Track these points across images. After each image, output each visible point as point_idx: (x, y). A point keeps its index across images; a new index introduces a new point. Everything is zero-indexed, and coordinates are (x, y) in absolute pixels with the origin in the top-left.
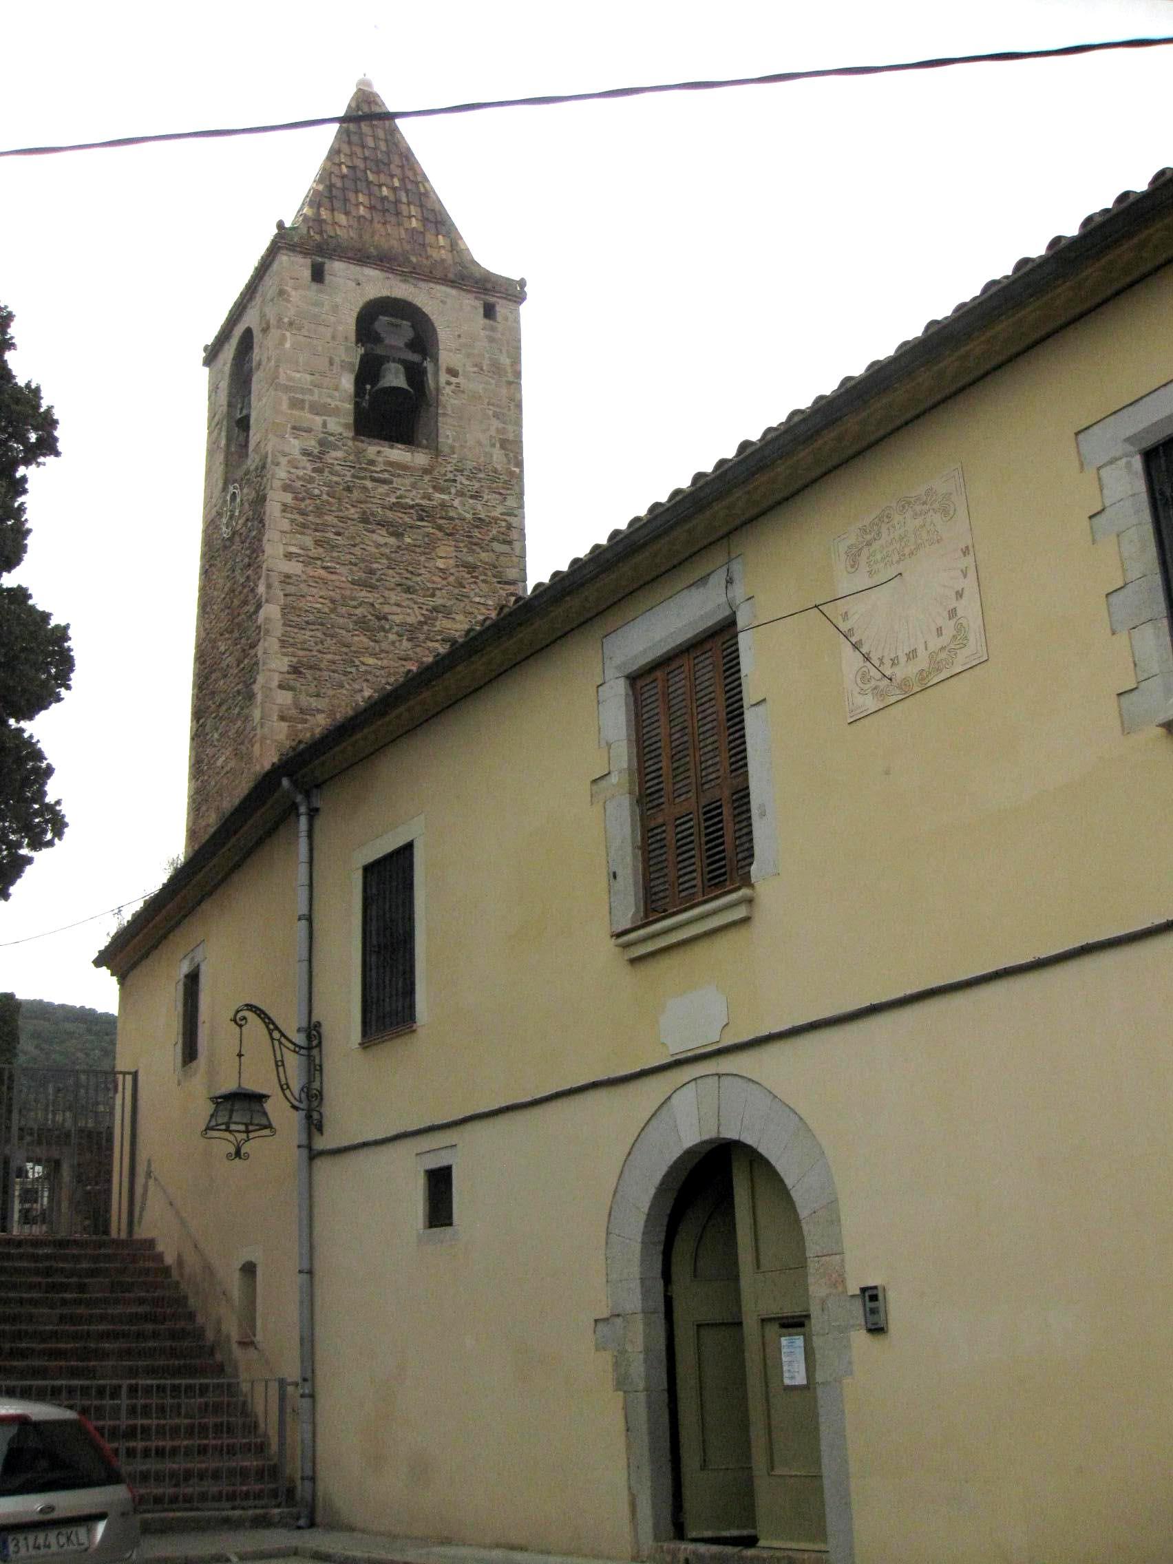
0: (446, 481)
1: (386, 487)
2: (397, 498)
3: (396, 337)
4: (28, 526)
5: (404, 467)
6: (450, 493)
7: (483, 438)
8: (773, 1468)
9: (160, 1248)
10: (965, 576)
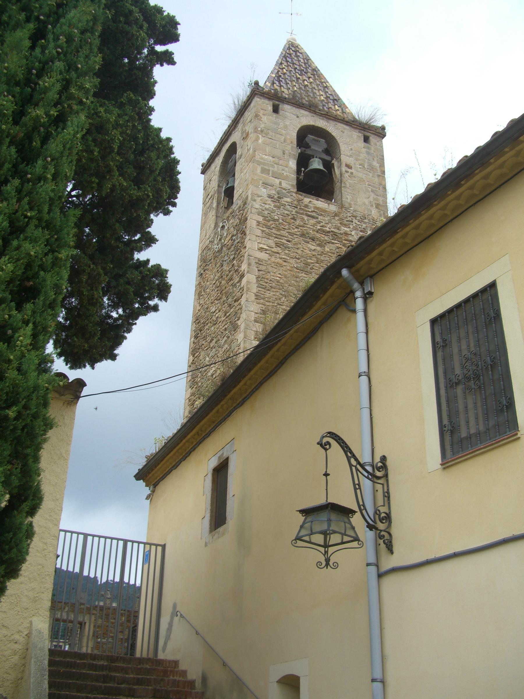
0: (347, 221)
5: (325, 211)
7: (367, 202)
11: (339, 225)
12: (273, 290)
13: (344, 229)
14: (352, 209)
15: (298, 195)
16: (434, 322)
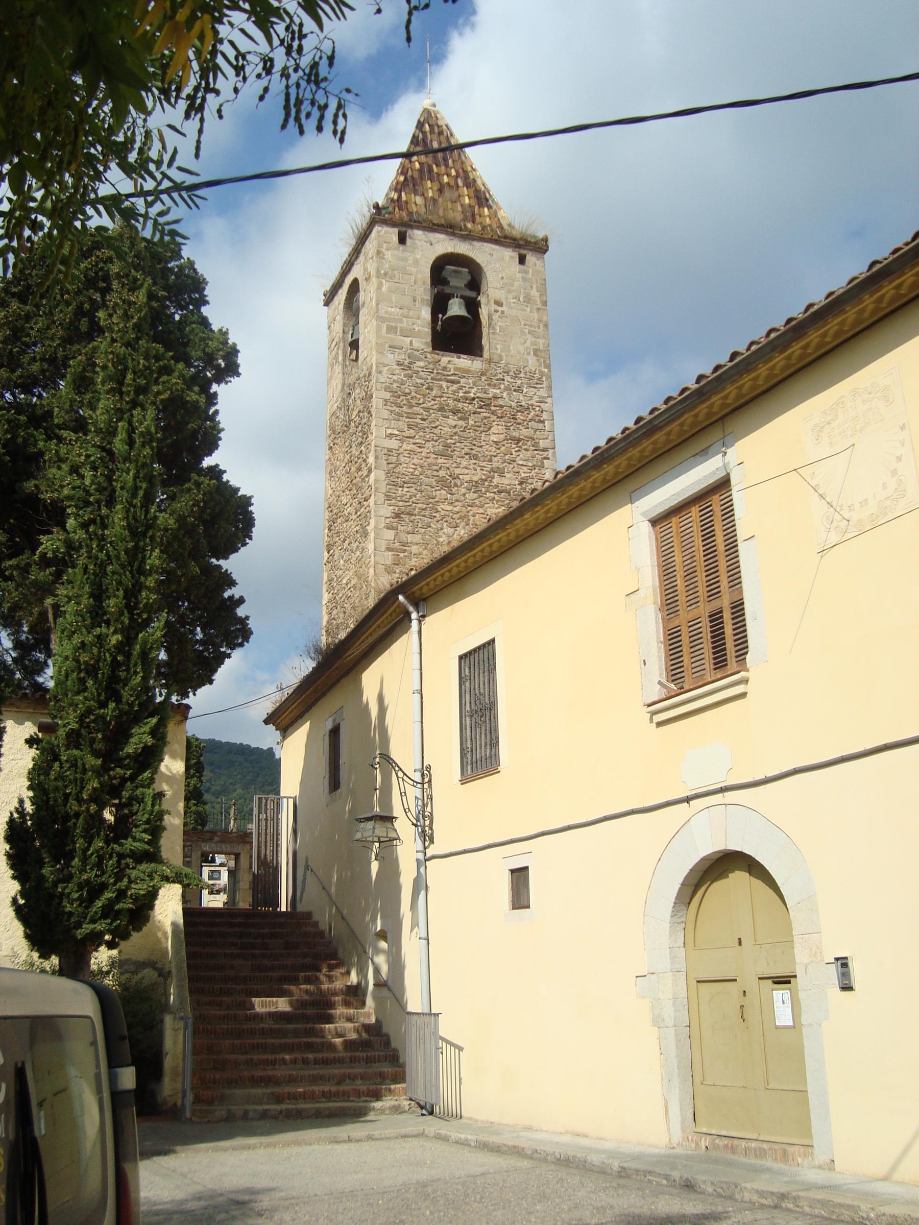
0: (497, 380)
1: (455, 386)
2: (465, 393)
3: (458, 280)
4: (221, 426)
5: (468, 371)
6: (499, 388)
7: (521, 348)
8: (768, 1085)
9: (316, 917)
10: (903, 445)
11: (487, 387)
12: (406, 485)
13: (493, 391)
14: (503, 362)
15: (433, 355)
16: (461, 658)
